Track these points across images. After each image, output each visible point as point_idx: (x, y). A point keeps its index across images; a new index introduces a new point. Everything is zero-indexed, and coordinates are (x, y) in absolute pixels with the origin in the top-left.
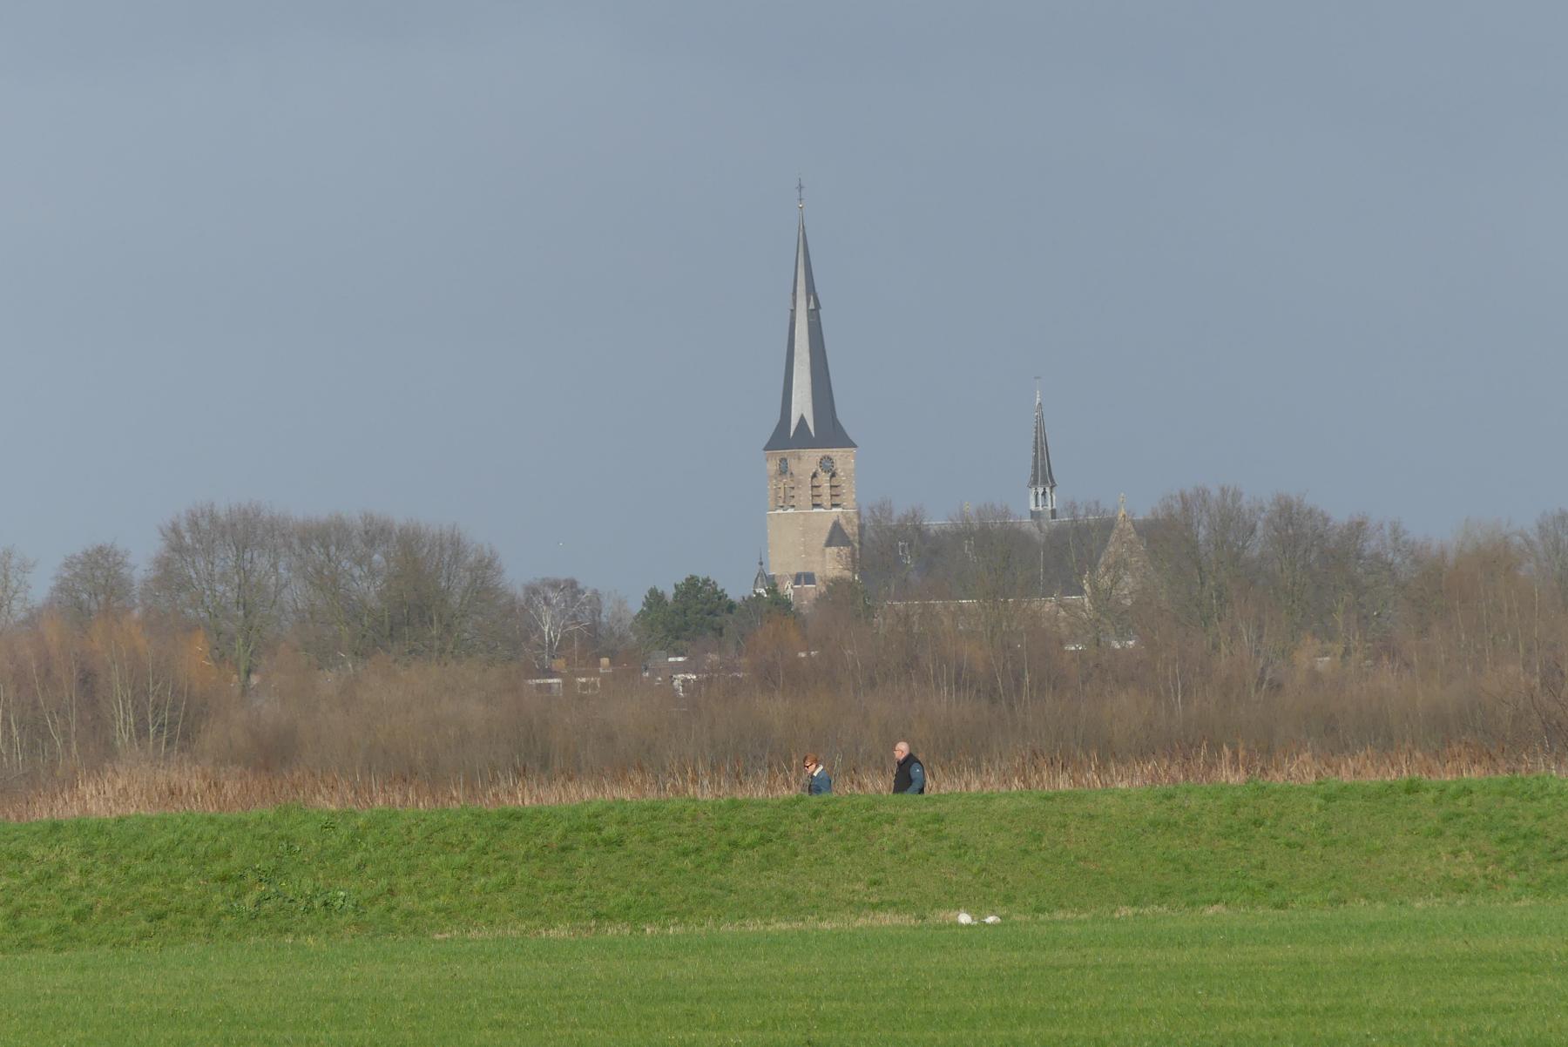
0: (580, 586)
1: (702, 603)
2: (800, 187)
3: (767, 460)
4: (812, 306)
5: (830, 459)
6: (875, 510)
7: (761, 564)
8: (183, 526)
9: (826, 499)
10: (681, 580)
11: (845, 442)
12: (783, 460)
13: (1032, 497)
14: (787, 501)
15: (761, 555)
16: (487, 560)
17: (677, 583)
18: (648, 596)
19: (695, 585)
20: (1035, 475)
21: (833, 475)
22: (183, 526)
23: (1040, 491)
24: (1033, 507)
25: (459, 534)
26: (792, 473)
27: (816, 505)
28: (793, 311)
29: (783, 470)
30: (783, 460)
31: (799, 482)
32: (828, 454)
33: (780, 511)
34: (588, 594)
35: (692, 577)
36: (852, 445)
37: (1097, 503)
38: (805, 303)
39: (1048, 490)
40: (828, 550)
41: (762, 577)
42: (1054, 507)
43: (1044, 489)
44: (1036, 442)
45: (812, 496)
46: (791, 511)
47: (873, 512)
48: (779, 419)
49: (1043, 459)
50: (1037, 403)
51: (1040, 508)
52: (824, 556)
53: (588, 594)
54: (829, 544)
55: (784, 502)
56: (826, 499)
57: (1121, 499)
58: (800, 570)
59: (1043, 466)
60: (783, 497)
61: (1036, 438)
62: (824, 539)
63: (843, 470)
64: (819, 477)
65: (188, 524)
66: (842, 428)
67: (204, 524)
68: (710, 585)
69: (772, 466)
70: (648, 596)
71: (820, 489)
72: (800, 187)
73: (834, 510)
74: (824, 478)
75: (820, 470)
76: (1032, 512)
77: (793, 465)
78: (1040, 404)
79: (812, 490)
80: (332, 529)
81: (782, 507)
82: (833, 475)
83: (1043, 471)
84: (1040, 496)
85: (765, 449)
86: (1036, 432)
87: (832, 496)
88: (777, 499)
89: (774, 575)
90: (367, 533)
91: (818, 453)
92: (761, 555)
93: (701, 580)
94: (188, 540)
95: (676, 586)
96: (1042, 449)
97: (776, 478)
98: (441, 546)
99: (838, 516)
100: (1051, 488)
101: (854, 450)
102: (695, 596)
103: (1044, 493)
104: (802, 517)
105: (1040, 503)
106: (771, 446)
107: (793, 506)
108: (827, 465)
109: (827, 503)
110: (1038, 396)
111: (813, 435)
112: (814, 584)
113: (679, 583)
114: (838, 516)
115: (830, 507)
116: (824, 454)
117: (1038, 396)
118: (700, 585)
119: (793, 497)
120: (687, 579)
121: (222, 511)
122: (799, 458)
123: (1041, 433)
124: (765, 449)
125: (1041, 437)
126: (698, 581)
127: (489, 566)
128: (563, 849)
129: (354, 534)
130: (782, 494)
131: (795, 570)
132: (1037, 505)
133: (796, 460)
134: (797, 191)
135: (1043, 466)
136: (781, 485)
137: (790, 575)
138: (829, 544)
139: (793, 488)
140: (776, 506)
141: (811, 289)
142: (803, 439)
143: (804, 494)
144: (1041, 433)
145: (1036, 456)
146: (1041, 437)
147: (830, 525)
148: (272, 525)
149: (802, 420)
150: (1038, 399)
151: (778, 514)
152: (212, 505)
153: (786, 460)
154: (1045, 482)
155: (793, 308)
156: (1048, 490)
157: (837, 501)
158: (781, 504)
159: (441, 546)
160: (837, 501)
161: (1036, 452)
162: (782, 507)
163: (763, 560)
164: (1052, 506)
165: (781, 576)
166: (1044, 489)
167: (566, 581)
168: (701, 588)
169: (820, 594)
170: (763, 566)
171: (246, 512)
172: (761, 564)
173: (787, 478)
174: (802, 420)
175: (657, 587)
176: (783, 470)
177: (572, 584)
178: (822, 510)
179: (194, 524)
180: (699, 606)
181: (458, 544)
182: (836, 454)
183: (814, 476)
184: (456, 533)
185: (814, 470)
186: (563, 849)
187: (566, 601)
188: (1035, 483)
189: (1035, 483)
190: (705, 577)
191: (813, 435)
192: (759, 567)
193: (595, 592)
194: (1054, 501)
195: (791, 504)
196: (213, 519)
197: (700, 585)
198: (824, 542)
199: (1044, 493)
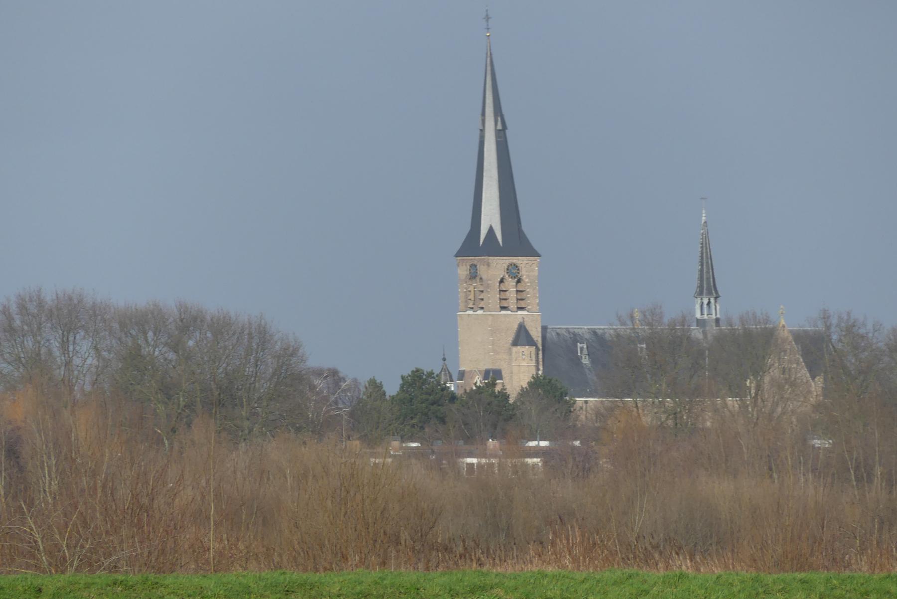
0: (341, 375)
1: (427, 393)
2: (487, 18)
3: (458, 266)
4: (500, 127)
5: (516, 266)
6: (647, 314)
7: (444, 359)
8: (14, 308)
9: (512, 303)
10: (407, 372)
11: (530, 251)
12: (473, 266)
13: (698, 307)
14: (477, 303)
15: (444, 350)
16: (291, 349)
17: (404, 375)
18: (367, 385)
19: (420, 377)
20: (701, 287)
21: (519, 281)
22: (14, 308)
23: (706, 301)
24: (698, 315)
25: (830, 324)
26: (481, 278)
27: (504, 308)
28: (482, 131)
29: (473, 275)
30: (473, 266)
31: (488, 286)
32: (514, 261)
33: (470, 312)
34: (348, 382)
35: (418, 370)
36: (536, 254)
37: (849, 314)
38: (493, 123)
39: (712, 300)
40: (515, 349)
41: (445, 371)
42: (718, 316)
43: (709, 299)
44: (702, 257)
45: (500, 299)
46: (480, 312)
47: (645, 315)
48: (469, 228)
49: (708, 272)
50: (703, 222)
51: (705, 317)
52: (511, 354)
53: (348, 382)
54: (515, 343)
55: (474, 304)
56: (512, 303)
57: (781, 311)
58: (489, 366)
59: (708, 279)
60: (473, 299)
61: (702, 253)
62: (510, 339)
63: (528, 276)
64: (506, 283)
65: (18, 307)
66: (528, 241)
67: (32, 308)
68: (434, 378)
69: (463, 271)
70: (367, 385)
71: (507, 293)
72: (487, 18)
73: (520, 312)
74: (510, 284)
75: (507, 276)
76: (697, 320)
77: (482, 270)
78: (705, 222)
79: (500, 294)
80: (150, 316)
81: (472, 308)
82: (519, 281)
83: (708, 283)
84: (705, 306)
85: (456, 256)
86: (702, 247)
87: (518, 299)
88: (467, 300)
89: (464, 371)
90: (182, 320)
91: (505, 261)
92: (444, 350)
93: (425, 373)
94: (18, 322)
95: (403, 378)
96: (707, 263)
97: (466, 282)
98: (250, 334)
99: (523, 319)
100: (716, 298)
101: (538, 259)
102: (421, 388)
103: (709, 303)
104: (490, 318)
105: (705, 312)
106: (461, 253)
107: (482, 308)
108: (514, 272)
109: (513, 306)
110: (704, 215)
111: (481, 242)
112: (502, 379)
113: (405, 374)
114: (523, 319)
115: (515, 309)
116: (511, 261)
117: (704, 215)
118: (424, 377)
119: (482, 299)
120: (413, 372)
121: (49, 298)
122: (488, 265)
123: (706, 249)
124: (456, 256)
125: (707, 252)
126: (423, 374)
127: (294, 353)
128: (889, 508)
129: (170, 321)
130: (472, 297)
131: (484, 367)
132: (702, 314)
133: (486, 266)
134: (484, 20)
135: (708, 279)
136: (471, 289)
137: (479, 371)
138: (515, 343)
139: (482, 291)
140: (466, 307)
141: (498, 111)
142: (491, 248)
143: (492, 298)
144: (706, 249)
145: (701, 271)
146: (707, 252)
147: (516, 326)
148: (94, 312)
149: (491, 231)
150: (704, 218)
151: (469, 315)
152: (40, 290)
153: (476, 266)
154: (709, 293)
155: (482, 128)
156: (712, 300)
157: (522, 304)
158: (472, 306)
159: (250, 334)
160: (522, 304)
161: (702, 265)
162: (472, 308)
163: (446, 357)
164: (716, 315)
165: (471, 372)
166: (709, 299)
167: (329, 370)
168: (425, 379)
169: (522, 390)
170: (446, 362)
171: (70, 299)
172: (444, 359)
173: (476, 283)
174: (491, 231)
175: (376, 378)
176: (473, 275)
177: (334, 373)
178: (509, 312)
179: (23, 308)
180: (424, 397)
181: (265, 334)
182: (522, 262)
183: (502, 281)
184: (263, 322)
185: (502, 276)
186: (889, 508)
187: (329, 388)
188: (700, 293)
189: (700, 293)
190: (429, 370)
191: (481, 242)
192: (442, 361)
193: (355, 380)
194: (717, 311)
195: (480, 306)
196: (41, 304)
197: (424, 377)
198: (511, 342)
199: (709, 303)
